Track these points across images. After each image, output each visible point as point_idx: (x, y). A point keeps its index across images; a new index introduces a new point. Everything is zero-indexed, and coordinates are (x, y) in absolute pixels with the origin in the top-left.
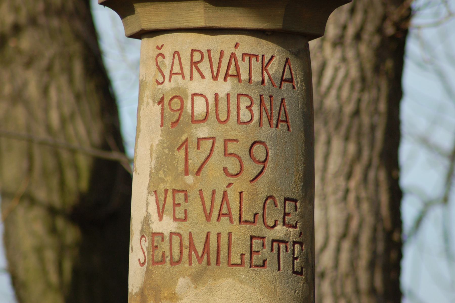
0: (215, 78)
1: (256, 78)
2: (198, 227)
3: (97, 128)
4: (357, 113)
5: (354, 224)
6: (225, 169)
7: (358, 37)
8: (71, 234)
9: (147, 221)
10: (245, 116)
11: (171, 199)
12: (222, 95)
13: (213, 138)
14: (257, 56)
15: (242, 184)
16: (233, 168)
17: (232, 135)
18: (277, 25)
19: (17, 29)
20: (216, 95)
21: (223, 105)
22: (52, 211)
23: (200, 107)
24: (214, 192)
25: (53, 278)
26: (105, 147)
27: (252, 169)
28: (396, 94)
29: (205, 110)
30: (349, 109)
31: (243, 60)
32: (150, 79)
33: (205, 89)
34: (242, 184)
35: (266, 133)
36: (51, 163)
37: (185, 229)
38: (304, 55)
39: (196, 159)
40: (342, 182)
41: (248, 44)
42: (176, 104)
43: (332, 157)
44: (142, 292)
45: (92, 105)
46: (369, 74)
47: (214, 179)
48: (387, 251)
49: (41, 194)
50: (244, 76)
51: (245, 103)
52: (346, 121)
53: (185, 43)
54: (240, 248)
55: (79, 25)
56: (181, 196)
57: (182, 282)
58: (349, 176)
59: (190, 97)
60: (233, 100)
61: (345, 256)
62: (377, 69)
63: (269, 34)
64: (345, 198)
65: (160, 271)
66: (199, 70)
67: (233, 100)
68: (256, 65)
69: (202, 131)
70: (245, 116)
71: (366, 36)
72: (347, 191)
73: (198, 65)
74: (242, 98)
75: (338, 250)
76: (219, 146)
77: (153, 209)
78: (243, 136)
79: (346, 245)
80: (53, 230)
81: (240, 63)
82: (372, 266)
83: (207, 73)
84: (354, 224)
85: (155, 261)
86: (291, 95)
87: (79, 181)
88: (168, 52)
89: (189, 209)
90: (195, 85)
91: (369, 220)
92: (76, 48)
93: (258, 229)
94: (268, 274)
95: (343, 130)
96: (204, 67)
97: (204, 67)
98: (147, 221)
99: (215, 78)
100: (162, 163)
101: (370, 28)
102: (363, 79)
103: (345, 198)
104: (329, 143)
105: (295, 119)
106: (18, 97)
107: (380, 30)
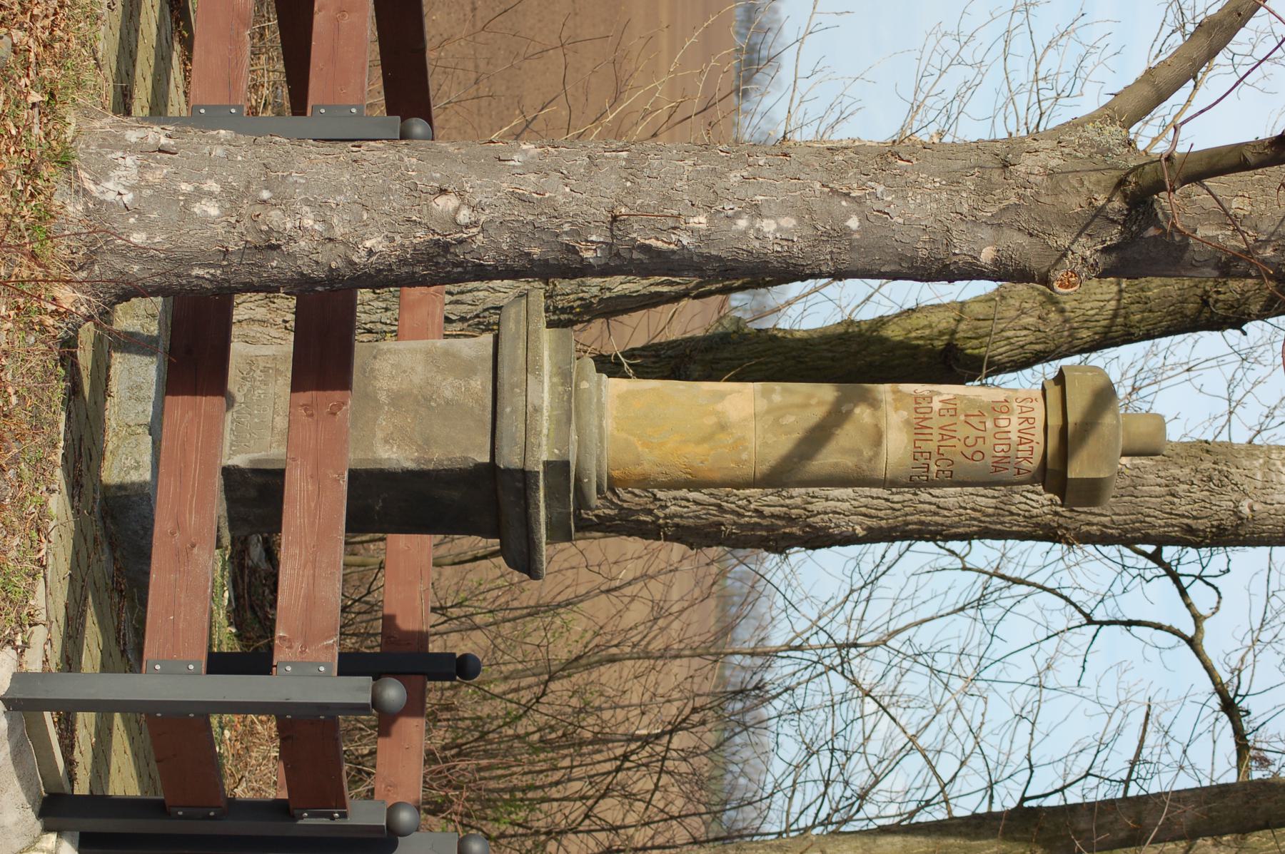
1: (1020, 454)
2: (935, 422)
3: (1004, 358)
4: (1012, 514)
5: (946, 513)
7: (1056, 513)
8: (939, 344)
9: (939, 394)
10: (998, 448)
11: (951, 407)
15: (960, 446)
16: (970, 442)
17: (987, 441)
18: (1049, 466)
19: (1062, 311)
21: (1004, 435)
22: (954, 332)
23: (1003, 423)
25: (913, 334)
26: (990, 364)
27: (968, 452)
28: (1022, 537)
30: (1013, 509)
32: (1018, 395)
33: (1013, 425)
34: (960, 446)
35: (989, 460)
36: (981, 331)
37: (935, 415)
38: (1032, 481)
39: (973, 421)
40: (971, 505)
41: (1039, 450)
42: (1004, 409)
43: (985, 499)
44: (899, 391)
45: (1017, 355)
46: (1034, 520)
47: (963, 431)
48: (930, 532)
49: (962, 326)
50: (1021, 447)
51: (1006, 448)
52: (1007, 507)
53: (1039, 414)
54: (925, 446)
55: (1118, 330)
56: (952, 412)
57: (905, 413)
58: (973, 509)
61: (927, 507)
62: (1037, 525)
64: (961, 507)
65: (911, 401)
68: (1027, 454)
69: (989, 424)
70: (998, 448)
71: (1056, 518)
72: (965, 508)
75: (930, 503)
77: (945, 397)
78: (987, 448)
79: (933, 508)
80: (941, 333)
82: (922, 523)
84: (946, 513)
85: (917, 399)
86: (1009, 474)
87: (971, 348)
88: (1034, 404)
90: (1015, 420)
91: (948, 522)
92: (1051, 346)
93: (935, 456)
94: (910, 462)
95: (1002, 506)
96: (1026, 425)
97: (1026, 425)
98: (939, 394)
100: (972, 402)
101: (1061, 521)
102: (1032, 517)
103: (961, 507)
104: (994, 497)
105: (997, 476)
106: (1023, 312)
107: (1060, 526)
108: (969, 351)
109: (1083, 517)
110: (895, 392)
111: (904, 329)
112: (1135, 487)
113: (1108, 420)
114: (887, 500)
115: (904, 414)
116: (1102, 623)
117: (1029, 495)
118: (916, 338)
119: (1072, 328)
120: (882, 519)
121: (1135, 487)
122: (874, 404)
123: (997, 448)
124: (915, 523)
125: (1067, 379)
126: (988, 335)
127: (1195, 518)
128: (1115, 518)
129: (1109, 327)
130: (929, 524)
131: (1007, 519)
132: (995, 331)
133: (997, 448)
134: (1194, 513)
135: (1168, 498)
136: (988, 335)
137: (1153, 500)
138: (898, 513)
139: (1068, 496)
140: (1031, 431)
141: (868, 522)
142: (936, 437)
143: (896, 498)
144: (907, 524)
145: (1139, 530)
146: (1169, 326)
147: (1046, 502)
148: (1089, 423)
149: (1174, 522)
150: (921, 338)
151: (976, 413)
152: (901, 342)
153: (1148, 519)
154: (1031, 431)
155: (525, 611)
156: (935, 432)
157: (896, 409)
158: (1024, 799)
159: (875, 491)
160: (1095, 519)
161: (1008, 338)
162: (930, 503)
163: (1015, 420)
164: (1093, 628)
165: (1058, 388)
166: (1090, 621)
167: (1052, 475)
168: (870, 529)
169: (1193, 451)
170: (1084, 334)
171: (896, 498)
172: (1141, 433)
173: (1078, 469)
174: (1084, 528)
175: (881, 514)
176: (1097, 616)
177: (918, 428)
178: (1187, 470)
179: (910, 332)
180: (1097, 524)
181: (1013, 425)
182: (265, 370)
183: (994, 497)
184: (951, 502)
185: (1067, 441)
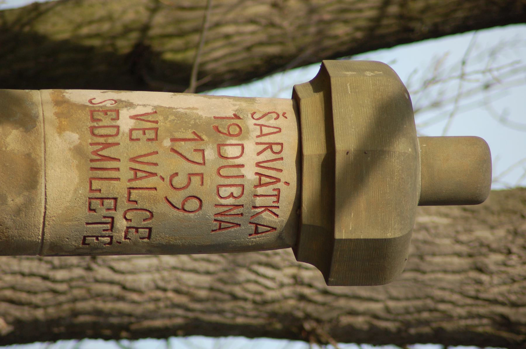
0: (258, 165)
1: (259, 201)
2: (124, 150)
3: (220, 67)
4: (235, 297)
5: (135, 297)
6: (177, 174)
7: (302, 298)
8: (125, 45)
9: (130, 105)
11: (149, 127)
12: (243, 171)
13: (204, 164)
14: (278, 201)
16: (178, 181)
20: (243, 166)
21: (234, 172)
22: (145, 28)
23: (232, 151)
24: (156, 164)
25: (85, 31)
26: (201, 75)
27: (177, 198)
29: (229, 156)
30: (238, 290)
31: (274, 190)
32: (255, 107)
33: (248, 156)
35: (209, 211)
36: (187, 26)
37: (123, 139)
38: (280, 243)
39: (186, 148)
40: (173, 285)
41: (289, 194)
42: (234, 130)
43: (194, 273)
45: (241, 60)
46: (269, 308)
48: (111, 326)
49: (159, 18)
50: (260, 191)
51: (236, 191)
52: (227, 288)
54: (106, 188)
55: (390, 25)
58: (177, 291)
59: (240, 142)
60: (238, 181)
61: (106, 288)
62: (273, 315)
63: (298, 212)
64: (158, 288)
65: (85, 116)
66: (264, 150)
67: (238, 181)
69: (210, 154)
70: (225, 192)
71: (302, 305)
72: (165, 290)
73: (269, 150)
74: (240, 189)
75: (112, 283)
76: (197, 169)
78: (206, 191)
79: (116, 290)
80: (127, 30)
81: (272, 187)
82: (98, 312)
84: (135, 297)
85: (94, 113)
86: (243, 233)
88: (281, 122)
89: (140, 143)
90: (251, 147)
91: (139, 310)
92: (291, 48)
94: (83, 213)
95: (220, 286)
96: (268, 155)
97: (268, 155)
98: (130, 105)
99: (258, 165)
100: (181, 118)
101: (310, 308)
102: (265, 303)
103: (158, 288)
104: (208, 273)
107: (308, 317)
108: (169, 56)
109: (342, 302)
110: (58, 103)
111: (71, 22)
112: (421, 257)
113: (401, 146)
114: (45, 278)
115: (74, 137)
117: (262, 270)
118: (90, 36)
119: (321, 22)
120: (36, 307)
121: (421, 257)
122: (27, 122)
123: (225, 192)
124: (88, 313)
125: (333, 81)
126: (198, 30)
127: (514, 305)
128: (392, 304)
129: (377, 21)
130: (109, 314)
131: (228, 306)
132: (207, 25)
134: (513, 298)
135: (474, 274)
136: (198, 30)
137: (450, 277)
138: (62, 298)
139: (335, 267)
140: (277, 165)
141: (16, 312)
142: (125, 174)
143: (60, 275)
144: (75, 314)
145: (426, 323)
146: (466, 18)
147: (286, 281)
148: (371, 154)
149: (482, 311)
150: (97, 35)
152: (65, 42)
153: (442, 307)
154: (277, 165)
156: (124, 166)
157: (61, 130)
159: (28, 264)
160: (361, 306)
161: (227, 36)
162: (112, 283)
163: (251, 147)
165: (318, 97)
167: (311, 235)
168: (18, 323)
169: (511, 204)
170: (341, 30)
171: (60, 275)
172: (452, 169)
173: (352, 225)
174: (345, 320)
175: (36, 299)
177: (96, 162)
178: (501, 233)
179: (79, 26)
180: (363, 314)
181: (248, 156)
183: (208, 273)
184: (143, 280)
185: (333, 182)
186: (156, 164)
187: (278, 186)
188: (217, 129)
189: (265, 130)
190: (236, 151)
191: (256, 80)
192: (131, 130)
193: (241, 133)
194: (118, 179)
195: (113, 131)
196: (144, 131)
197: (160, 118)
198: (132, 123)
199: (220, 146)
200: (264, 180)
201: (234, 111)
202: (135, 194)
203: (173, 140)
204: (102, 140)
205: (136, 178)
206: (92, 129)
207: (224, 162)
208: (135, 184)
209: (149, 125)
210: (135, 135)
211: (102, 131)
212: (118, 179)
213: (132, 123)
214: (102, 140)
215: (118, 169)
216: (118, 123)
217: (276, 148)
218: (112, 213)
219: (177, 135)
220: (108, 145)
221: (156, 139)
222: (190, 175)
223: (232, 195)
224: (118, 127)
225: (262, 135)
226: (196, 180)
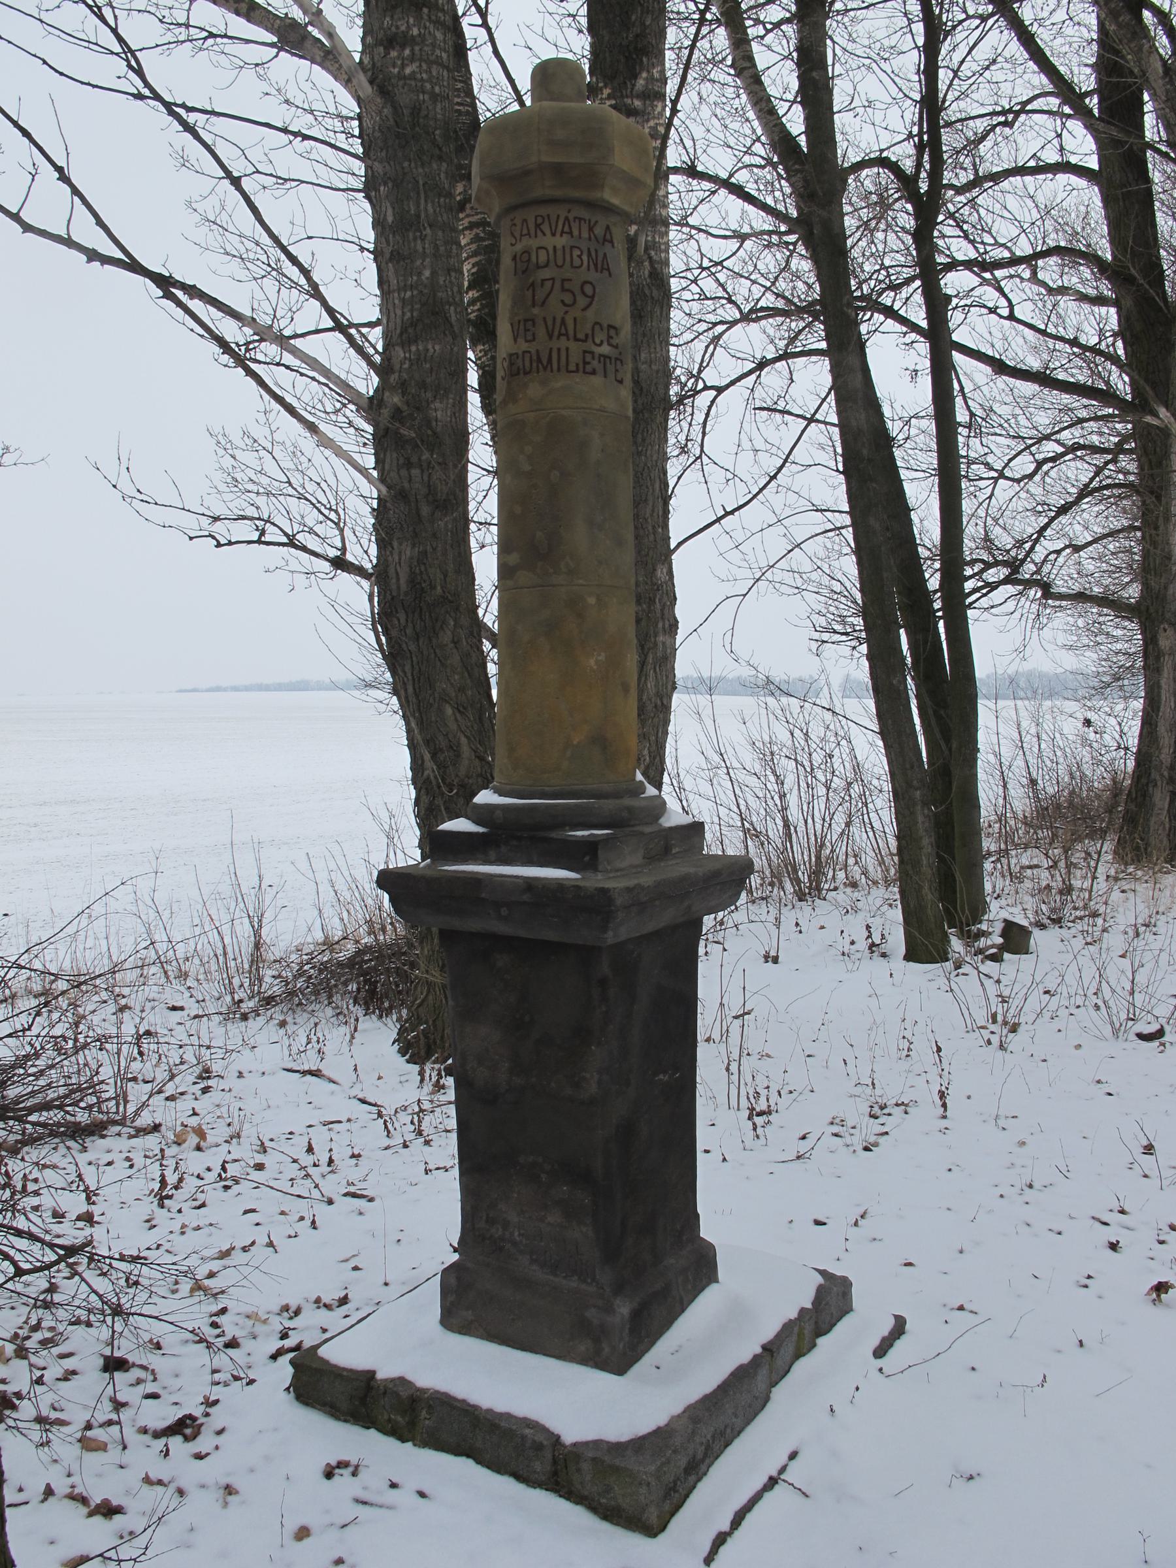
0: (554, 235)
6: (562, 301)
12: (559, 246)
16: (568, 299)
21: (560, 253)
23: (543, 257)
24: (554, 319)
39: (540, 294)
50: (576, 233)
60: (568, 250)
67: (568, 250)
68: (585, 228)
69: (546, 274)
81: (572, 224)
83: (548, 232)
88: (518, 221)
99: (554, 235)
116: (702, 451)
133: (577, 262)
151: (529, 293)
155: (196, 305)
158: (838, 471)
164: (704, 457)
166: (700, 457)
176: (698, 453)
182: (491, 1221)
186: (554, 319)
187: (571, 218)
188: (524, 272)
189: (525, 232)
190: (542, 253)
191: (325, 1412)
192: (526, 341)
193: (527, 252)
194: (567, 349)
195: (527, 356)
196: (526, 330)
197: (517, 319)
198: (521, 340)
199: (538, 267)
200: (566, 229)
201: (202, 1425)
202: (581, 336)
203: (534, 305)
204: (535, 365)
205: (567, 335)
206: (526, 373)
207: (552, 264)
208: (571, 333)
209: (522, 327)
210: (529, 338)
211: (527, 364)
212: (567, 349)
213: (521, 340)
214: (535, 365)
215: (559, 350)
216: (520, 353)
217: (539, 220)
218: (597, 356)
219: (530, 303)
220: (539, 360)
221: (533, 321)
222: (563, 290)
223: (580, 257)
224: (524, 352)
225: (529, 234)
226: (567, 285)
